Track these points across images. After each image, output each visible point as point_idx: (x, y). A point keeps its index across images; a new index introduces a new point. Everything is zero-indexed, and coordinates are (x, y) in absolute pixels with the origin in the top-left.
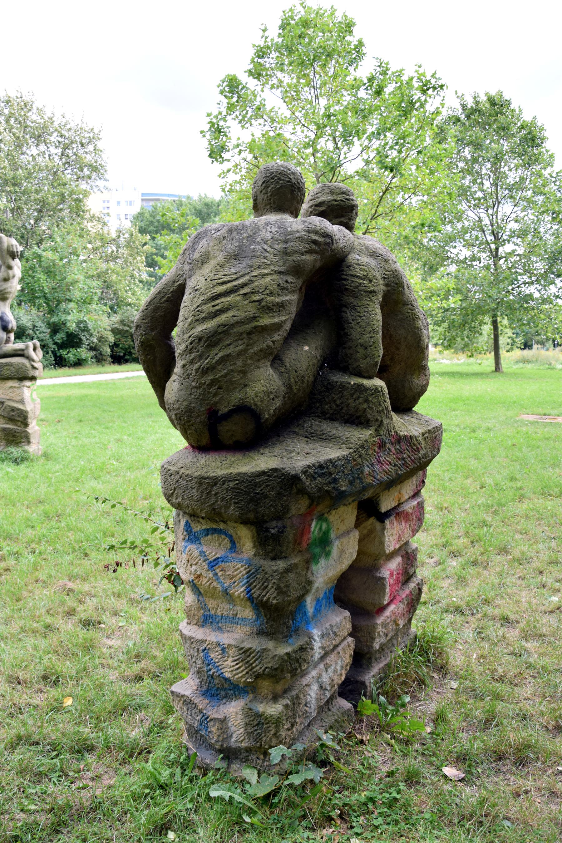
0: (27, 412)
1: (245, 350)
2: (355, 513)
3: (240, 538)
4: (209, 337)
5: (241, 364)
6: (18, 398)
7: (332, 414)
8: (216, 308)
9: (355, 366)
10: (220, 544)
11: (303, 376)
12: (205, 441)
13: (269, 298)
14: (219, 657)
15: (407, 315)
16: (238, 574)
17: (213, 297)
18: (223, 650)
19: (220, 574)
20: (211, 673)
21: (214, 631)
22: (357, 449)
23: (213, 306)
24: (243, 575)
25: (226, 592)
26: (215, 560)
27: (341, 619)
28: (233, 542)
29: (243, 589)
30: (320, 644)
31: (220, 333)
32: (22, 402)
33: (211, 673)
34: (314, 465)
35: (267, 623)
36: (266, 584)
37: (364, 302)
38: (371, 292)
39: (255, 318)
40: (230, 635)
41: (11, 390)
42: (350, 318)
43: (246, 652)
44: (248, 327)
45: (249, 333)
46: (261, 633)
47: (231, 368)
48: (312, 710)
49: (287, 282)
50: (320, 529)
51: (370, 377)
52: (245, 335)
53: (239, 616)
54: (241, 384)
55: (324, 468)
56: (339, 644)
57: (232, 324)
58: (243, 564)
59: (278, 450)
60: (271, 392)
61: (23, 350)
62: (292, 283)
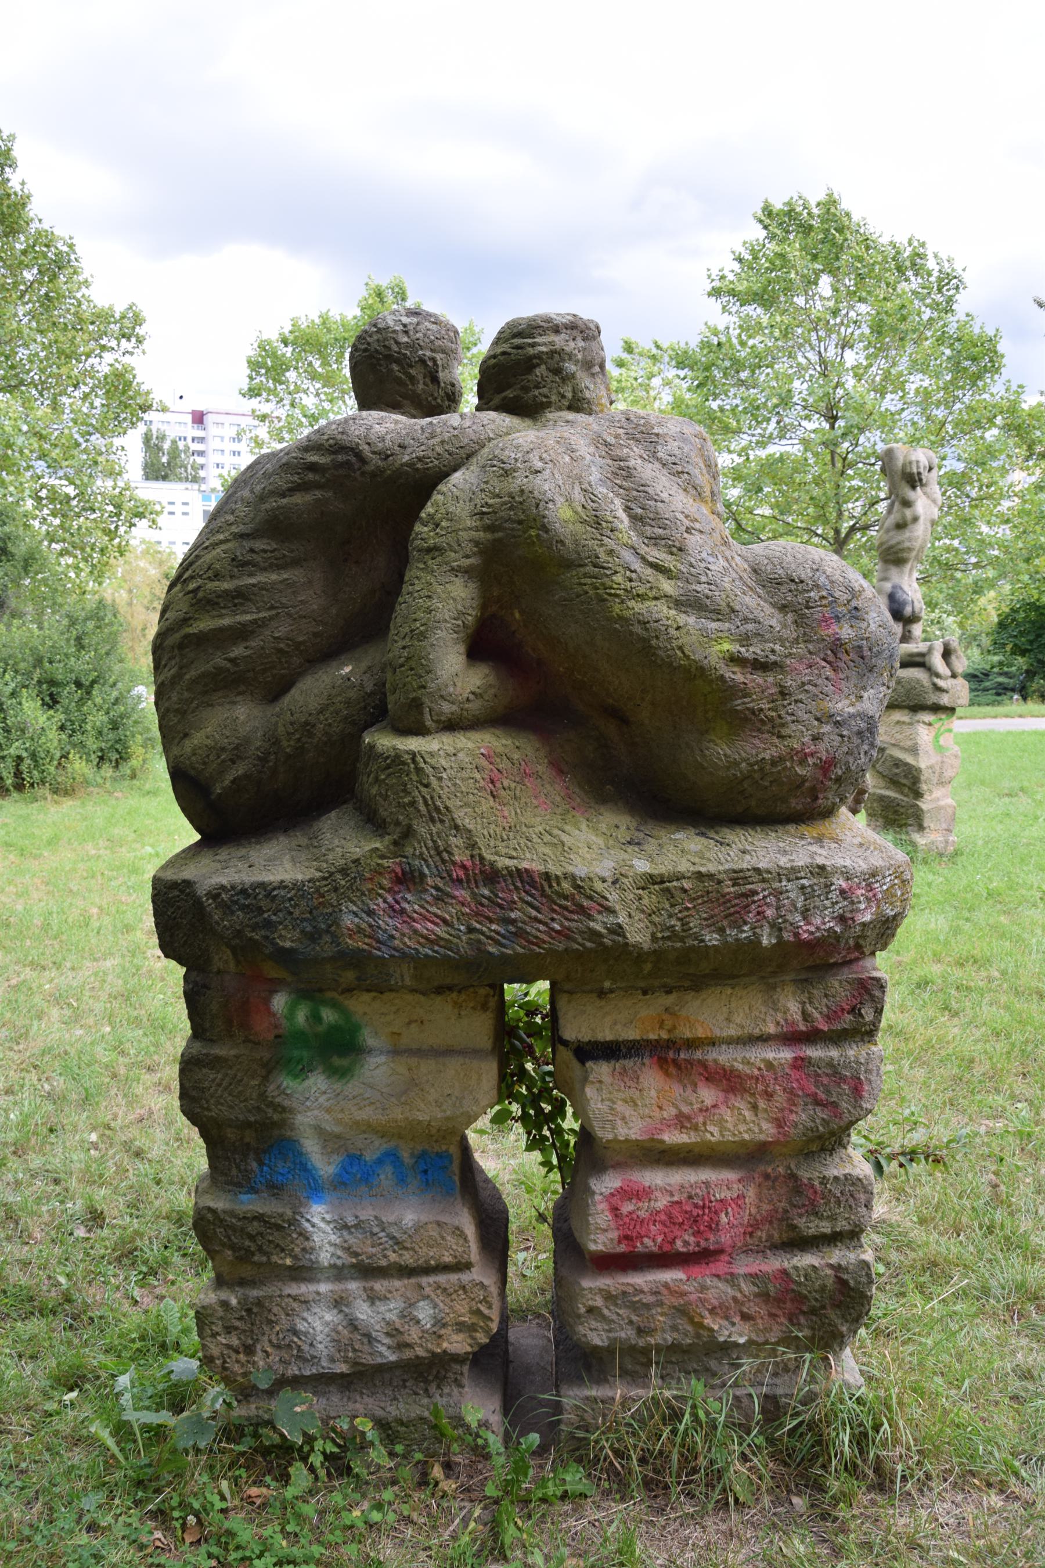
0: (919, 770)
6: (909, 743)
13: (211, 585)
15: (578, 589)
22: (331, 874)
32: (914, 750)
34: (233, 888)
38: (429, 550)
41: (897, 728)
49: (252, 550)
55: (248, 896)
60: (223, 749)
61: (922, 655)
62: (265, 551)
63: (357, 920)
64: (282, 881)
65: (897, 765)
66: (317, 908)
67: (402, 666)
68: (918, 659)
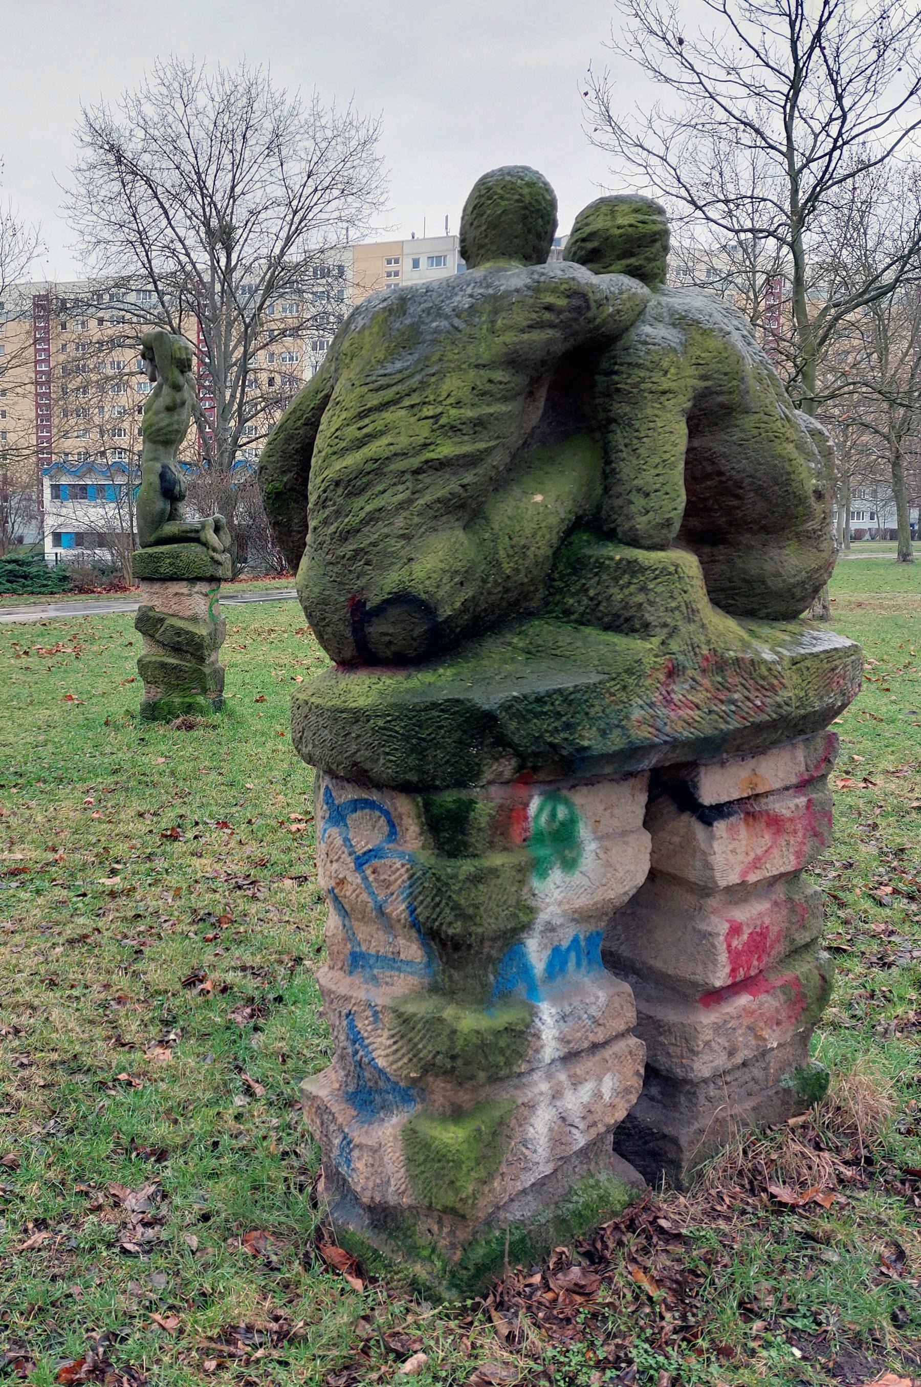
1: (410, 501)
2: (643, 798)
3: (400, 817)
4: (350, 481)
5: (402, 525)
6: (189, 613)
7: (582, 614)
8: (365, 431)
9: (627, 526)
10: (374, 827)
11: (524, 547)
12: (348, 653)
14: (369, 1028)
16: (396, 880)
17: (360, 413)
18: (376, 1013)
19: (371, 879)
20: (358, 1058)
21: (366, 982)
22: (619, 674)
23: (360, 429)
24: (404, 881)
25: (380, 910)
26: (365, 854)
27: (603, 998)
28: (391, 824)
29: (403, 907)
30: (556, 1033)
31: (369, 473)
33: (358, 1058)
34: (525, 697)
35: (444, 971)
36: (437, 899)
37: (649, 411)
38: (664, 393)
39: (426, 445)
40: (388, 990)
41: (176, 599)
42: (622, 441)
43: (406, 1021)
44: (415, 462)
45: (417, 472)
46: (434, 989)
47: (386, 530)
48: (542, 1161)
49: (490, 381)
50: (553, 815)
51: (662, 547)
52: (408, 476)
53: (402, 956)
54: (402, 557)
56: (606, 1044)
57: (387, 458)
58: (404, 861)
59: (466, 668)
61: (197, 531)
62: (501, 383)
63: (643, 712)
64: (576, 686)
65: (178, 634)
66: (608, 706)
67: (656, 491)
68: (193, 535)
